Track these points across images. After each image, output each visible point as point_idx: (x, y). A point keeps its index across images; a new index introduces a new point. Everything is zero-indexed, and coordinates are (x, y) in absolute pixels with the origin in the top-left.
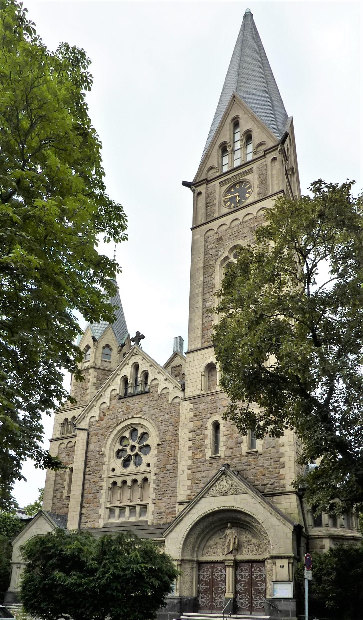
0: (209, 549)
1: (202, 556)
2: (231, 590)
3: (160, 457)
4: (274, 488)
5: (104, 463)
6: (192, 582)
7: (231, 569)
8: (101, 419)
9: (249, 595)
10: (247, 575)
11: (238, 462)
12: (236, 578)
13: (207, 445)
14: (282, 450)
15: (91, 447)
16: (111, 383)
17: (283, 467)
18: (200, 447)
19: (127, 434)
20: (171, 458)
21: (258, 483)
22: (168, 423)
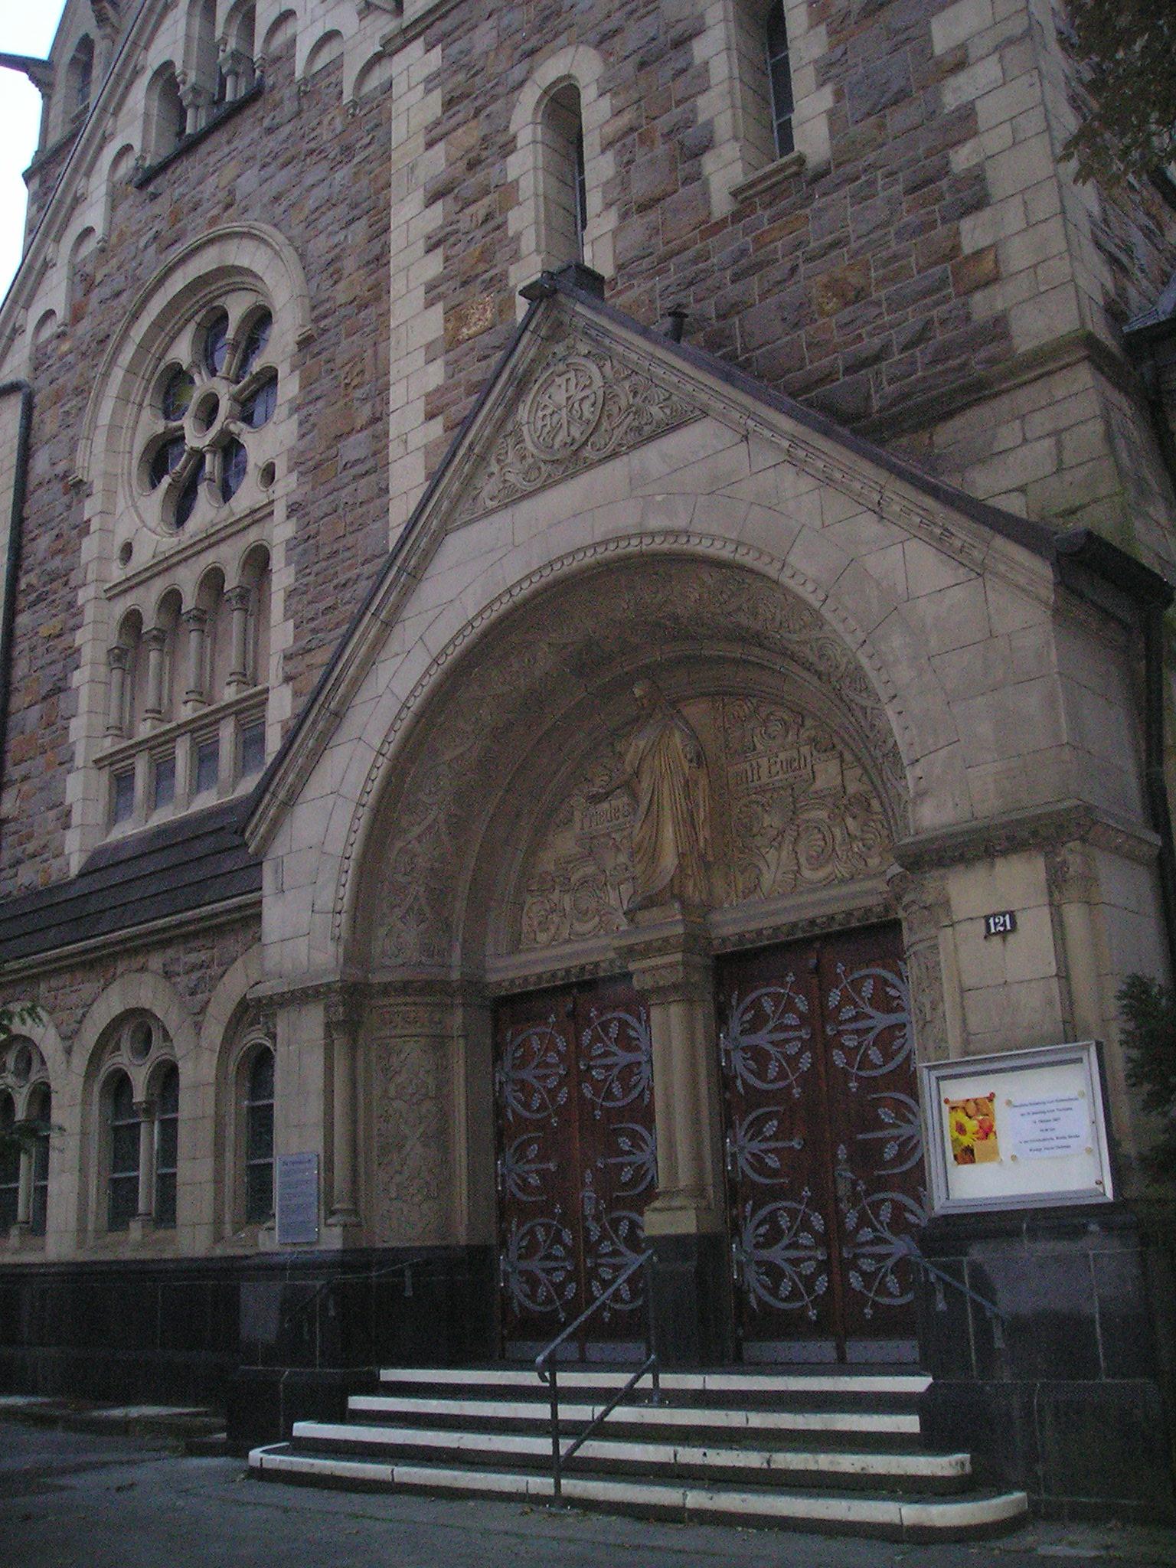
0: (555, 896)
1: (515, 947)
2: (685, 1179)
3: (311, 409)
4: (934, 362)
5: (84, 529)
6: (441, 1137)
7: (676, 1011)
8: (77, 314)
9: (815, 1204)
10: (792, 1049)
11: (690, 272)
12: (724, 1080)
13: (518, 236)
14: (955, 93)
15: (40, 465)
16: (109, 123)
17: (980, 203)
18: (481, 267)
19: (183, 352)
20: (359, 393)
21: (821, 364)
22: (342, 210)
